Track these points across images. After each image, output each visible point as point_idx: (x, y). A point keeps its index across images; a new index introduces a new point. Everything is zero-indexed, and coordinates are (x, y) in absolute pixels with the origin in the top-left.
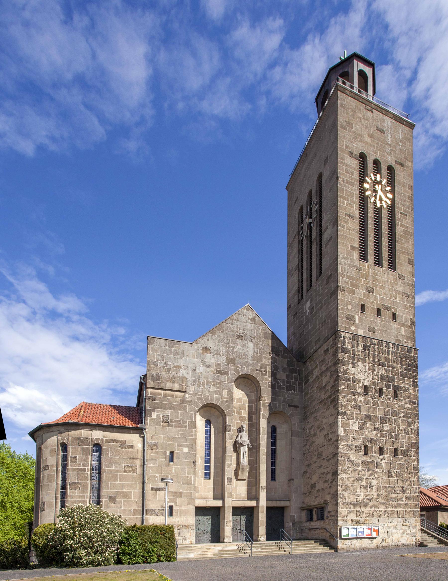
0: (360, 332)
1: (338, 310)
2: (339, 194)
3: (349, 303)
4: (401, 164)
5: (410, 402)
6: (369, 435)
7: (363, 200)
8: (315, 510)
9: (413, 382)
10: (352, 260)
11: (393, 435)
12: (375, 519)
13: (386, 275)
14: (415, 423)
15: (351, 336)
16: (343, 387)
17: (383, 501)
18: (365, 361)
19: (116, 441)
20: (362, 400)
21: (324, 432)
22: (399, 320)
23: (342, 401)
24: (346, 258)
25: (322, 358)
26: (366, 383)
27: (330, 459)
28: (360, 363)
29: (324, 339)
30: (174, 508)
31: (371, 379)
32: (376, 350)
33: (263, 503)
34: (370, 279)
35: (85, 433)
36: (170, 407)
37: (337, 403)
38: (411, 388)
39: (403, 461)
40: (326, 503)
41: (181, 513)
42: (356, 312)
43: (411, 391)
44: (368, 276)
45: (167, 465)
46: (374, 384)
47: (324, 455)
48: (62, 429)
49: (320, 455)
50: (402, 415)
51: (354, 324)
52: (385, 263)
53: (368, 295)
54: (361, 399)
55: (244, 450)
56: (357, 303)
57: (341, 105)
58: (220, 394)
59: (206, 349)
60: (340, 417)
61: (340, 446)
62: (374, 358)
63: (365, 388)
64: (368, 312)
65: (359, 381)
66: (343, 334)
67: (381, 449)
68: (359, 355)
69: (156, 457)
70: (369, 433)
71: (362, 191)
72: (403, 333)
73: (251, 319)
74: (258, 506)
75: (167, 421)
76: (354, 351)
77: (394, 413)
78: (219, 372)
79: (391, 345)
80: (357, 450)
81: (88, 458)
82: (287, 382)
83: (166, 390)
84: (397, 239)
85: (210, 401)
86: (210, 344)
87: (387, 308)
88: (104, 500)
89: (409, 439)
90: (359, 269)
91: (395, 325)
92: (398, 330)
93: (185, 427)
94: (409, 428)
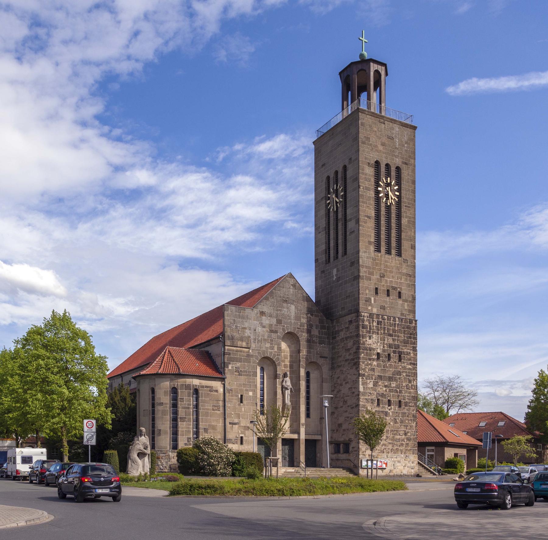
0: (375, 311)
1: (359, 295)
2: (361, 200)
3: (367, 288)
4: (406, 164)
5: (411, 364)
6: (381, 390)
7: (378, 200)
8: (341, 446)
9: (414, 347)
10: (369, 253)
11: (398, 390)
12: (385, 455)
13: (394, 261)
14: (414, 380)
15: (368, 315)
16: (363, 355)
17: (390, 441)
18: (378, 334)
19: (207, 387)
20: (376, 364)
21: (349, 386)
22: (403, 297)
23: (362, 366)
24: (365, 252)
25: (347, 326)
26: (379, 351)
27: (353, 408)
28: (374, 336)
29: (349, 311)
30: (244, 438)
31: (382, 347)
32: (386, 324)
33: (303, 436)
34: (382, 267)
35: (189, 381)
36: (240, 360)
37: (359, 367)
38: (411, 352)
39: (405, 411)
40: (350, 440)
41: (248, 443)
42: (371, 294)
43: (412, 355)
44: (381, 264)
45: (239, 405)
46: (384, 351)
47: (349, 403)
48: (173, 377)
49: (345, 402)
50: (405, 374)
51: (370, 305)
52: (393, 252)
53: (381, 280)
54: (375, 363)
55: (288, 392)
56: (373, 287)
57: (362, 123)
58: (272, 349)
59: (262, 313)
60: (360, 378)
61: (361, 400)
62: (384, 331)
63: (378, 354)
64: (380, 293)
65: (374, 349)
66: (363, 314)
67: (389, 401)
68: (374, 329)
69: (232, 399)
70: (381, 389)
71: (377, 192)
72: (406, 308)
73: (292, 285)
74: (299, 439)
75: (239, 372)
76: (370, 326)
77: (399, 373)
78: (271, 331)
79: (397, 319)
80: (372, 403)
81: (190, 399)
82: (320, 337)
83: (237, 347)
84: (402, 229)
85: (266, 355)
86: (265, 309)
87: (395, 288)
88: (201, 431)
89: (410, 393)
90: (374, 259)
91: (400, 302)
92: (403, 305)
93: (250, 376)
94: (410, 385)
